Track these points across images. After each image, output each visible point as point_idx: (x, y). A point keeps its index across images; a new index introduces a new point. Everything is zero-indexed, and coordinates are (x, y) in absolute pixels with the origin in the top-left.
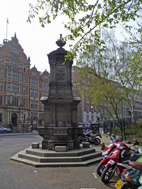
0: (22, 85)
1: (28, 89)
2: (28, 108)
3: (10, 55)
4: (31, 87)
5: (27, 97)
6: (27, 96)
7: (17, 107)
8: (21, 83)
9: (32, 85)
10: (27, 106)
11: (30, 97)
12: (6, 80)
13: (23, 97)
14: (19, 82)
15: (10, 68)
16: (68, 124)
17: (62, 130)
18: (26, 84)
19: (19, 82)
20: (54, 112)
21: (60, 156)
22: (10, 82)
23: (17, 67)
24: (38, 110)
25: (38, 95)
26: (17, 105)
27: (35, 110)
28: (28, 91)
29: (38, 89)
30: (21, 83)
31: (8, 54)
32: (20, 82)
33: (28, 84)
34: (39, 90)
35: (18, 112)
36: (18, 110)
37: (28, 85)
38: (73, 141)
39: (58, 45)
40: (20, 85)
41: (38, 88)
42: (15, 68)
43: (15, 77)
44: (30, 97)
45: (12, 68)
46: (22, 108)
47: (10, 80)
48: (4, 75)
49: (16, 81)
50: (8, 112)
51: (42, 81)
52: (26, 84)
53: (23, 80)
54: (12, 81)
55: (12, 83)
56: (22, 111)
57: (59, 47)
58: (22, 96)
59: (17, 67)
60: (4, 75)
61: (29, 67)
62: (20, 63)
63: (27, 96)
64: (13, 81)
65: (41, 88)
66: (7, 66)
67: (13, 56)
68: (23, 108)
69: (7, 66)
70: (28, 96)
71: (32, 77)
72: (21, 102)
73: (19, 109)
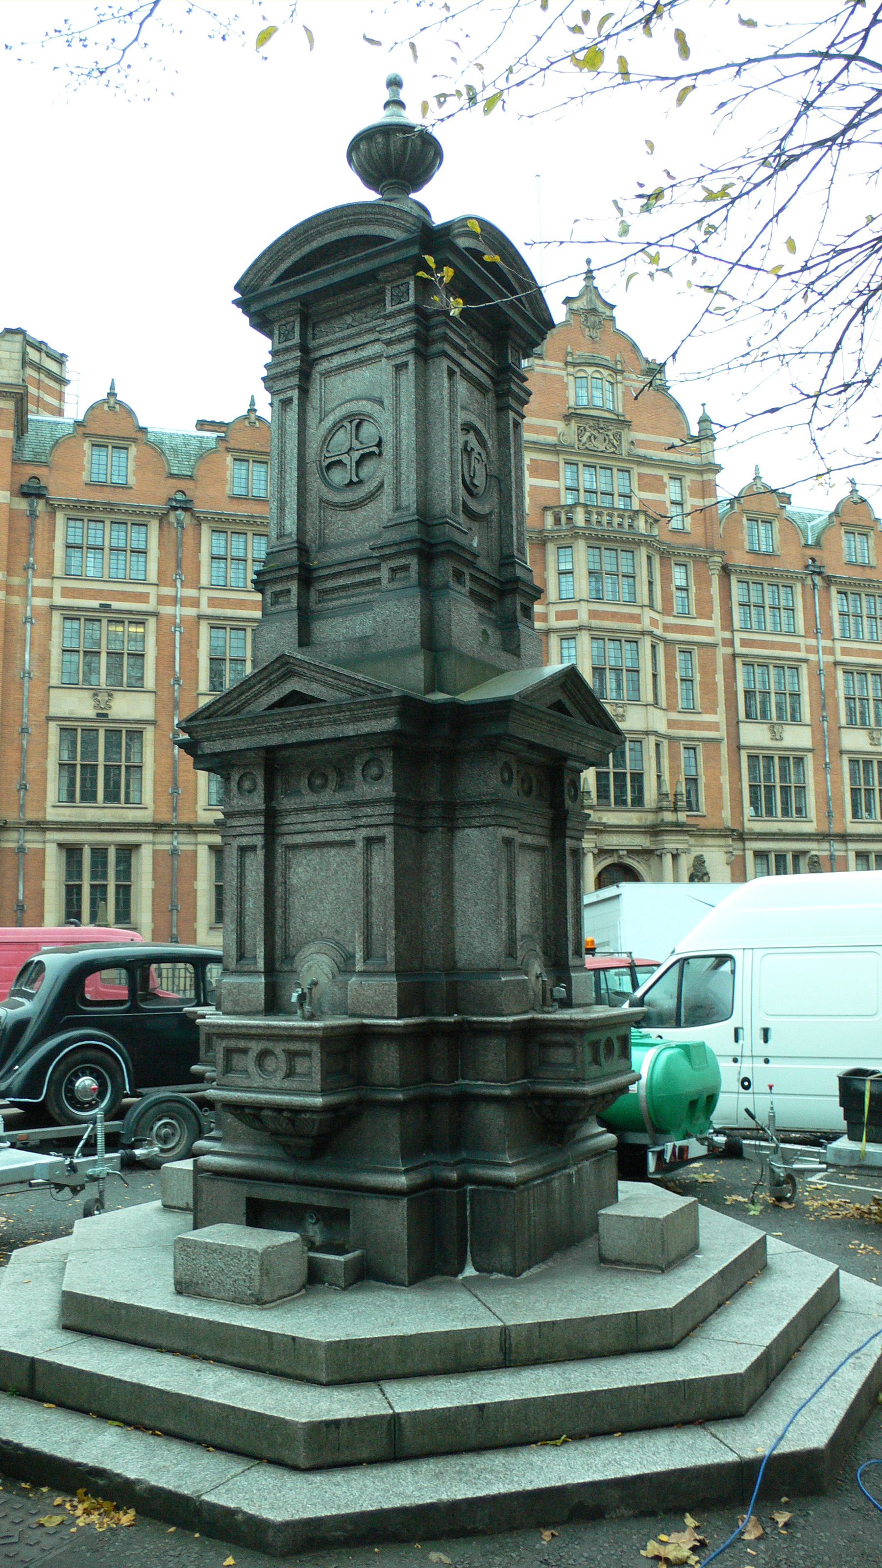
0: (670, 636)
1: (714, 662)
2: (726, 814)
3: (560, 426)
4: (744, 643)
5: (715, 726)
6: (707, 718)
7: (631, 818)
8: (654, 622)
9: (744, 630)
10: (716, 804)
11: (734, 725)
12: (196, 603)
13: (682, 733)
14: (636, 618)
15: (569, 519)
16: (367, 981)
17: (279, 1048)
18: (700, 622)
19: (636, 618)
20: (261, 853)
21: (179, 1344)
22: (638, 627)
23: (620, 503)
24: (809, 828)
25: (805, 699)
26: (638, 800)
27: (789, 827)
28: (720, 678)
29: (802, 655)
30: (654, 622)
31: (551, 423)
32: (648, 614)
33: (715, 622)
34: (812, 657)
35: (646, 853)
36: (641, 841)
37: (710, 632)
38: (402, 1181)
39: (371, 179)
40: (647, 642)
41: (796, 647)
42: (605, 519)
43: (782, 596)
44: (734, 725)
45: (580, 518)
46: (669, 816)
47: (573, 615)
48: (692, 596)
49: (614, 616)
50: (668, 859)
51: (829, 580)
52: (700, 622)
53: (667, 599)
54: (583, 617)
55: (590, 629)
56: (671, 843)
57: (364, 194)
58: (671, 724)
59: (620, 503)
60: (692, 596)
61: (707, 489)
62: (636, 470)
63: (707, 718)
64: (593, 614)
65: (825, 643)
66: (546, 509)
67: (581, 431)
68: (682, 817)
69: (546, 509)
70: (720, 717)
71: (740, 559)
72: (666, 777)
73: (655, 831)
